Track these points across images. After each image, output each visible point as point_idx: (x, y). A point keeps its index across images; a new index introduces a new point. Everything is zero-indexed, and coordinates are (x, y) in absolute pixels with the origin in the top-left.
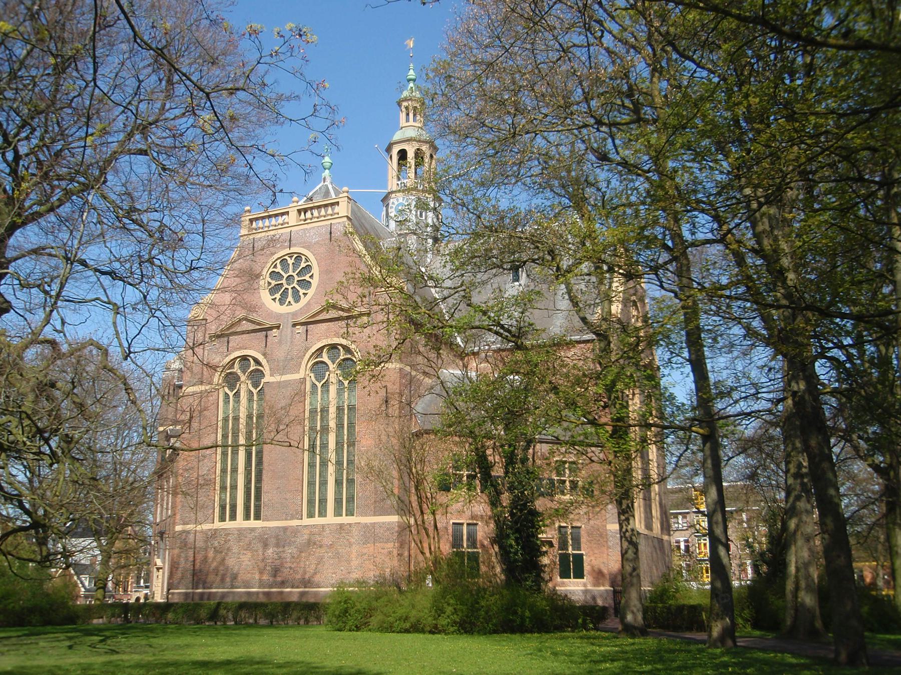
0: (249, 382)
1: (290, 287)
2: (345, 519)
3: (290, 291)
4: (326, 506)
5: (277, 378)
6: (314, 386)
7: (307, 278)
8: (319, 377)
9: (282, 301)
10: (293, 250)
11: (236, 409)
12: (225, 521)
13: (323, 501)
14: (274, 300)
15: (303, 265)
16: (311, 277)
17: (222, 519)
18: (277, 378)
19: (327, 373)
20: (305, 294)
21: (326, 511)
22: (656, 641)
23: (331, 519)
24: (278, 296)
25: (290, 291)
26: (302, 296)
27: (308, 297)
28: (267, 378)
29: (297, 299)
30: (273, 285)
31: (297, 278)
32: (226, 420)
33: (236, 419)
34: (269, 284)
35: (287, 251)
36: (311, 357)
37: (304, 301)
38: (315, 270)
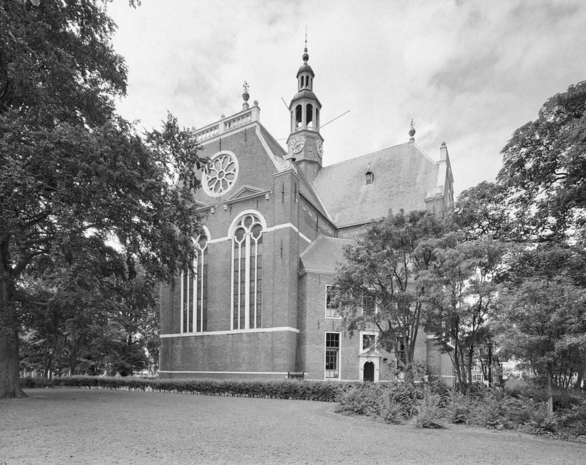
1: (221, 179)
2: (255, 330)
3: (221, 182)
6: (236, 244)
7: (232, 172)
8: (239, 239)
10: (223, 152)
11: (243, 254)
12: (237, 329)
14: (211, 189)
16: (235, 170)
17: (235, 327)
19: (244, 235)
20: (230, 183)
21: (244, 325)
23: (247, 329)
24: (213, 186)
25: (221, 182)
26: (229, 184)
27: (233, 185)
28: (209, 241)
29: (225, 186)
30: (210, 179)
31: (225, 173)
32: (236, 260)
33: (243, 259)
36: (233, 227)
37: (230, 187)
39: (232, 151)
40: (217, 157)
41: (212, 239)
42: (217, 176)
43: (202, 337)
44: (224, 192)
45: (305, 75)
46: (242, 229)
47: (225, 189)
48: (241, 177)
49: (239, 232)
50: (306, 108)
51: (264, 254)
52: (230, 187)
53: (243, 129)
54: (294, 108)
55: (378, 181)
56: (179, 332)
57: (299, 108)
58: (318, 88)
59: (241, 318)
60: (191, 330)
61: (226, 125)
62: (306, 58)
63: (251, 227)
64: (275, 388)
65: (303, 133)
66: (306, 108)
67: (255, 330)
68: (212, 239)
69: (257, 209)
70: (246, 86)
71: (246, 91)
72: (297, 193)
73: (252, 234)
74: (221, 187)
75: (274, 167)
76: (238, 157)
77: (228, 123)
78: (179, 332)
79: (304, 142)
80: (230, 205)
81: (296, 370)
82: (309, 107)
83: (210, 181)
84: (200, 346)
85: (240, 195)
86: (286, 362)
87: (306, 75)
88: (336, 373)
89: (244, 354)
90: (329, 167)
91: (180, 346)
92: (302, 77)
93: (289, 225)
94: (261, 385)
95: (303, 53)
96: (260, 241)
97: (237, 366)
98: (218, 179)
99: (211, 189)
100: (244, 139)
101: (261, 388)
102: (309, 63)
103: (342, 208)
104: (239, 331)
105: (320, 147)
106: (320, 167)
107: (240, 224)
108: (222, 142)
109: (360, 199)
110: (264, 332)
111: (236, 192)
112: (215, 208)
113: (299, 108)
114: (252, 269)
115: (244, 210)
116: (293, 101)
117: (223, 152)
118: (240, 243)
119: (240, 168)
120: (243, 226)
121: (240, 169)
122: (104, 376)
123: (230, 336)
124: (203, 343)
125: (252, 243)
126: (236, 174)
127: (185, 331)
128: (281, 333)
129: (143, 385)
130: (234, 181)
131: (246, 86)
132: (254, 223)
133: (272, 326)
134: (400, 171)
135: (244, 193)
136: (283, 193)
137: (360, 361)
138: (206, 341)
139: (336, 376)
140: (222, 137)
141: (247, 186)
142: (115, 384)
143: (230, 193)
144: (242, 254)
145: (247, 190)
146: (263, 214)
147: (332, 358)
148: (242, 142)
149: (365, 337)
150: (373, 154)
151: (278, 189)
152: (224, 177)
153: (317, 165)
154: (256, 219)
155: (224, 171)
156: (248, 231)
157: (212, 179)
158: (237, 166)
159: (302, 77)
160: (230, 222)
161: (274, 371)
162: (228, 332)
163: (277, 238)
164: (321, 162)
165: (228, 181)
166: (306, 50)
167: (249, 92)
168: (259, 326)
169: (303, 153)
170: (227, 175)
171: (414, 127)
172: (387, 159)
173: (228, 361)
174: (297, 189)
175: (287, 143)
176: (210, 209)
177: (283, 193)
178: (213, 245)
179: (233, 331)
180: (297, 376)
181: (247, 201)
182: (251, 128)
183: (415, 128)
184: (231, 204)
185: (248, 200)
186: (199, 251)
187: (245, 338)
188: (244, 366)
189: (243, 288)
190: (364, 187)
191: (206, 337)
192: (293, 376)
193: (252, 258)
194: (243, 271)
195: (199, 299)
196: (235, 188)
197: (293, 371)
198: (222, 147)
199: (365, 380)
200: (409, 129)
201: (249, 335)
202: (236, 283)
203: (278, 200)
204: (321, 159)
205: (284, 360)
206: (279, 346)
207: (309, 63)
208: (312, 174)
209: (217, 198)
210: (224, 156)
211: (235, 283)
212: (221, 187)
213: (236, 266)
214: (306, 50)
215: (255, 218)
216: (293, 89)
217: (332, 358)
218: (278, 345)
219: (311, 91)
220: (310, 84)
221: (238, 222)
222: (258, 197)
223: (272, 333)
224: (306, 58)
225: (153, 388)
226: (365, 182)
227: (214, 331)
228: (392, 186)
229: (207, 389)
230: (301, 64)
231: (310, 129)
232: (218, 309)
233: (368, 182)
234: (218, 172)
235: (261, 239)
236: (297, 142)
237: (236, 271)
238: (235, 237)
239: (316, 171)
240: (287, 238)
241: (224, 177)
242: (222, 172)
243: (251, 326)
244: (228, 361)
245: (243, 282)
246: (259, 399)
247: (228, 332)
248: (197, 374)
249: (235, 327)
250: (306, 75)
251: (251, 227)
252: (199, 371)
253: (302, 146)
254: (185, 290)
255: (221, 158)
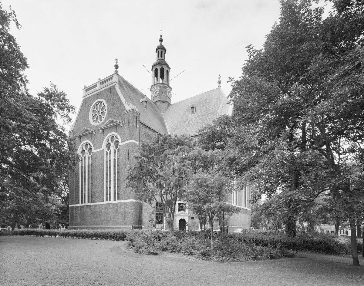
0: (88, 153)
1: (99, 115)
2: (117, 201)
3: (99, 117)
4: (111, 189)
5: (124, 143)
6: (107, 152)
7: (104, 111)
8: (108, 149)
9: (96, 121)
10: (99, 100)
11: (110, 158)
13: (110, 198)
15: (103, 106)
16: (105, 110)
18: (124, 143)
20: (103, 117)
22: (187, 209)
23: (112, 201)
24: (95, 119)
25: (99, 117)
27: (104, 118)
28: (93, 151)
29: (101, 119)
30: (93, 115)
31: (101, 112)
32: (107, 161)
33: (110, 161)
34: (92, 115)
35: (97, 101)
37: (103, 119)
38: (106, 108)
39: (104, 99)
40: (97, 102)
41: (94, 150)
42: (97, 113)
43: (90, 206)
44: (101, 122)
45: (160, 51)
46: (109, 143)
47: (101, 121)
48: (108, 114)
49: (108, 146)
50: (161, 70)
51: (120, 158)
52: (103, 119)
53: (109, 86)
54: (154, 70)
55: (198, 111)
56: (78, 203)
57: (156, 70)
58: (169, 59)
59: (109, 195)
60: (85, 202)
61: (101, 84)
62: (161, 40)
63: (114, 142)
64: (116, 234)
65: (158, 85)
66: (161, 70)
67: (117, 201)
68: (94, 150)
69: (116, 132)
70: (116, 60)
71: (116, 64)
72: (138, 123)
73: (114, 146)
74: (99, 120)
75: (125, 108)
76: (107, 102)
77: (102, 82)
78: (78, 203)
79: (159, 90)
80: (103, 130)
81: (139, 225)
82: (162, 69)
83: (93, 116)
84: (89, 211)
85: (108, 124)
86: (131, 220)
87: (161, 51)
88: (162, 225)
89: (111, 215)
90: (174, 104)
91: (79, 211)
92: (159, 52)
93: (132, 141)
94: (109, 233)
95: (160, 37)
96: (118, 151)
97: (107, 222)
98: (97, 115)
99: (94, 121)
100: (110, 92)
101: (109, 235)
102: (163, 43)
103: (177, 129)
104: (108, 202)
105: (169, 92)
106: (169, 104)
107: (108, 141)
108: (99, 94)
109: (187, 123)
110: (120, 203)
111: (106, 123)
112: (96, 132)
113: (156, 70)
114: (115, 166)
115: (110, 133)
116: (153, 66)
117: (99, 100)
118: (108, 152)
119: (108, 108)
120: (110, 142)
121: (108, 109)
122: (39, 230)
123: (104, 205)
124: (90, 210)
125: (115, 152)
126: (106, 112)
127: (82, 203)
128: (128, 203)
129: (55, 234)
130: (105, 116)
131: (116, 60)
132: (115, 140)
133: (124, 199)
134: (210, 105)
135: (110, 122)
136: (129, 122)
137: (177, 218)
138: (92, 208)
139: (163, 228)
140: (99, 91)
141: (111, 119)
142: (42, 234)
143: (103, 123)
144: (110, 158)
145: (112, 122)
146: (120, 135)
147: (160, 217)
148: (109, 93)
149: (179, 204)
150: (198, 96)
151: (127, 120)
152: (100, 114)
153: (167, 103)
154: (117, 138)
155: (100, 110)
156: (112, 144)
157: (95, 115)
158: (106, 108)
159: (159, 52)
160: (103, 140)
161: (125, 225)
162: (102, 203)
163: (127, 149)
164: (170, 101)
165: (102, 116)
166: (161, 36)
167: (118, 64)
168: (118, 199)
169: (158, 97)
170: (102, 112)
171: (220, 79)
172: (205, 98)
173: (103, 219)
174: (138, 120)
175: (151, 91)
176: (93, 133)
177: (129, 122)
178: (95, 153)
179: (105, 202)
180: (138, 228)
181: (111, 127)
182: (113, 86)
183: (221, 79)
184: (103, 130)
185: (112, 127)
186: (82, 158)
187: (111, 206)
188: (111, 222)
189: (110, 177)
190: (191, 116)
191: (92, 206)
192: (135, 228)
193: (115, 160)
194: (110, 167)
195: (88, 184)
196: (105, 120)
197: (136, 225)
198: (99, 98)
199: (179, 229)
200: (218, 80)
201: (113, 204)
202: (107, 175)
203: (127, 127)
204: (170, 99)
205: (131, 218)
206: (128, 210)
207: (163, 43)
208: (164, 108)
209: (96, 126)
210: (100, 102)
211: (106, 175)
212: (99, 120)
213: (107, 165)
214: (161, 36)
215: (116, 137)
216: (154, 59)
217: (160, 217)
218: (128, 210)
219: (164, 60)
220: (163, 55)
221: (107, 140)
222: (117, 125)
223: (125, 203)
224: (161, 40)
225: (60, 236)
226: (191, 113)
227: (96, 202)
228: (205, 115)
229: (84, 236)
230: (158, 44)
231: (164, 83)
232: (97, 190)
233: (193, 113)
234: (97, 111)
235: (119, 149)
236: (156, 90)
237: (107, 168)
238: (106, 148)
239: (166, 107)
240: (131, 148)
241: (100, 114)
242: (99, 111)
243: (115, 199)
244: (103, 219)
245: (110, 174)
246: (83, 240)
247: (102, 203)
248: (87, 227)
249: (107, 200)
250: (161, 51)
251: (114, 142)
252: (89, 225)
253: (158, 93)
254: (82, 179)
255: (99, 103)
